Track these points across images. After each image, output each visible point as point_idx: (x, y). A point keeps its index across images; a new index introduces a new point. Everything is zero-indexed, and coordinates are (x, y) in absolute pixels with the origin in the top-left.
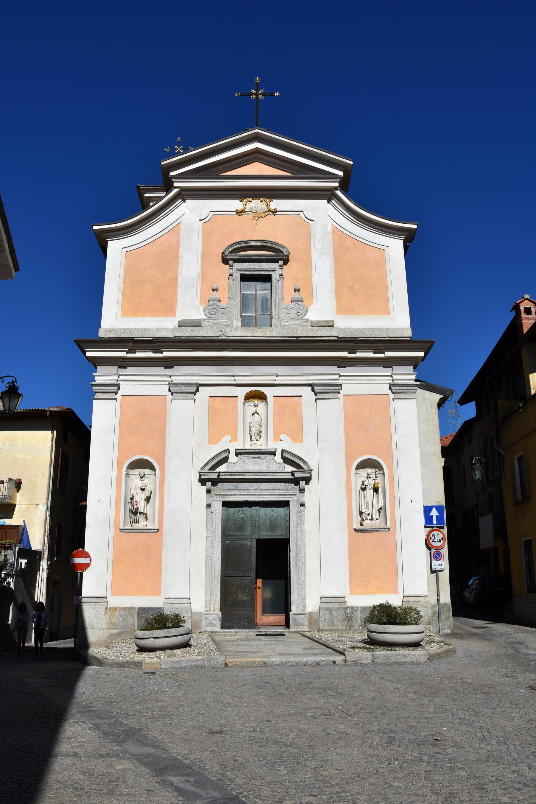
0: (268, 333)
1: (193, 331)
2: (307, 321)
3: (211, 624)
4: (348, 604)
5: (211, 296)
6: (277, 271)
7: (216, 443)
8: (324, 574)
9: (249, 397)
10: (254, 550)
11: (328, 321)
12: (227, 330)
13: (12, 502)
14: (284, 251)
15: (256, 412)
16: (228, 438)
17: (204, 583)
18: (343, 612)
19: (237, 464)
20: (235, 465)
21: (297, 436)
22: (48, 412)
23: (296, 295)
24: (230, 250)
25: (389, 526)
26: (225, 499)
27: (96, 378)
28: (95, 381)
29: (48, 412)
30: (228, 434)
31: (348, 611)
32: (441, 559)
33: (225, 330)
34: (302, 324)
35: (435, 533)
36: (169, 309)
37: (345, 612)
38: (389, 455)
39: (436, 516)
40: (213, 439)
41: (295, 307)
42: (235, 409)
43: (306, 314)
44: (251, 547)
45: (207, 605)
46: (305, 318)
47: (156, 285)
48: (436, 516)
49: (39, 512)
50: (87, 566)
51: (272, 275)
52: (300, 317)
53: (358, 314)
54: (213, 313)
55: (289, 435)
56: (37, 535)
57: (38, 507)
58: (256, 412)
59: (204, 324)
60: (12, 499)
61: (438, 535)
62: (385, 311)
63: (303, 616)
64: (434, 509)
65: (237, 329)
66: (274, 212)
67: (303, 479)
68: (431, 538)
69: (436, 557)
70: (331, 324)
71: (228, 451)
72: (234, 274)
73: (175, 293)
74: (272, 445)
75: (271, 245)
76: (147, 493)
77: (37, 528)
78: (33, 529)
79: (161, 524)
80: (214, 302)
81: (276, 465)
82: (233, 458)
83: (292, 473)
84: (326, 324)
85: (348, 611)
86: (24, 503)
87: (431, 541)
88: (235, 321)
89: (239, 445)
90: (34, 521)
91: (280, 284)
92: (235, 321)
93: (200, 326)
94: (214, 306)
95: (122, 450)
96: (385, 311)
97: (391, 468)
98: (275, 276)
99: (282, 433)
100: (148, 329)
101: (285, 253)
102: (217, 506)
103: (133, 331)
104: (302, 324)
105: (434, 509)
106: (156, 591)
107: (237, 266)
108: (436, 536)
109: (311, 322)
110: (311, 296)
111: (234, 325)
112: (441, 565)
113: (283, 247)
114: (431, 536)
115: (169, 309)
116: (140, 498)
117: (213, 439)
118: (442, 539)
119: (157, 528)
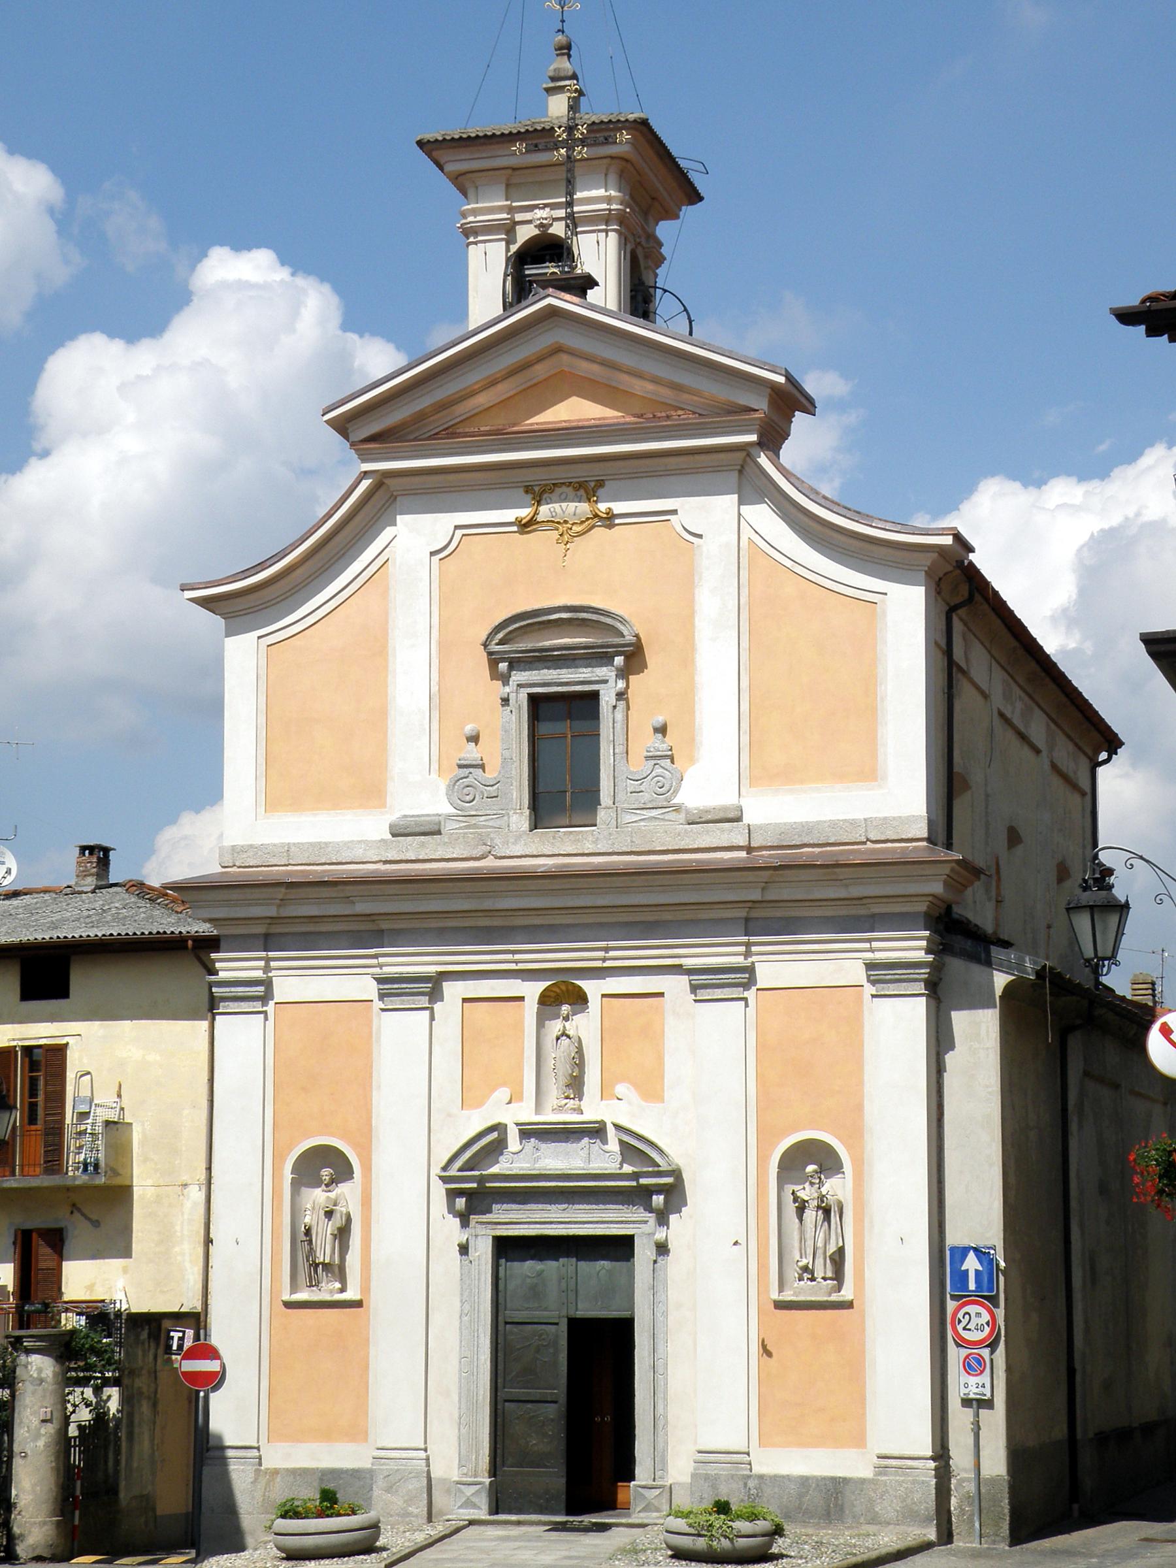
0: (588, 845)
1: (423, 845)
2: (678, 809)
3: (469, 1504)
4: (757, 1469)
5: (463, 755)
6: (612, 683)
7: (480, 1105)
8: (705, 1401)
9: (549, 1001)
10: (563, 1342)
11: (725, 809)
12: (498, 841)
13: (118, 1181)
14: (626, 633)
15: (564, 1034)
16: (503, 1094)
17: (456, 1416)
18: (741, 1484)
19: (521, 1155)
20: (519, 1159)
21: (651, 1088)
22: (190, 942)
23: (659, 744)
24: (500, 635)
25: (847, 1293)
26: (499, 1233)
27: (218, 965)
28: (216, 973)
29: (190, 942)
30: (504, 1084)
31: (751, 1484)
32: (982, 1372)
33: (492, 839)
34: (667, 817)
35: (972, 1309)
36: (371, 793)
37: (745, 1484)
38: (856, 1134)
39: (976, 1271)
40: (469, 1098)
41: (654, 774)
42: (519, 1026)
43: (676, 792)
44: (557, 1336)
45: (463, 1463)
46: (676, 801)
47: (327, 749)
48: (976, 1271)
49: (188, 1205)
50: (216, 1380)
51: (601, 692)
52: (664, 802)
53: (802, 782)
54: (468, 798)
55: (637, 1086)
56: (187, 1265)
57: (185, 1191)
58: (564, 1034)
59: (448, 827)
60: (115, 1173)
61: (978, 1315)
62: (868, 772)
63: (658, 1492)
64: (972, 1254)
65: (518, 838)
66: (609, 520)
67: (659, 1189)
68: (960, 1321)
69: (979, 1363)
70: (731, 815)
71: (499, 1128)
72: (512, 697)
73: (382, 746)
74: (592, 1110)
75: (594, 617)
76: (338, 1221)
77: (186, 1246)
78: (177, 1249)
79: (366, 1288)
80: (471, 770)
81: (604, 1159)
82: (514, 1142)
83: (635, 1176)
84: (721, 815)
85: (751, 1484)
86: (149, 1182)
87: (960, 1328)
88: (514, 818)
89: (525, 1112)
90: (178, 1228)
91: (619, 716)
92: (514, 818)
93: (439, 833)
94: (470, 780)
95: (282, 1126)
96: (868, 772)
97: (858, 1164)
98: (607, 698)
99: (622, 1081)
100: (326, 843)
101: (629, 638)
102: (483, 1250)
103: (293, 849)
104: (667, 817)
105: (972, 1254)
106: (357, 1432)
107: (518, 677)
108: (973, 1316)
109: (688, 812)
110: (691, 741)
111: (513, 827)
112: (983, 1386)
113: (623, 621)
114: (960, 1315)
115: (371, 793)
116: (324, 1233)
117: (469, 1098)
118: (988, 1323)
119: (357, 1297)
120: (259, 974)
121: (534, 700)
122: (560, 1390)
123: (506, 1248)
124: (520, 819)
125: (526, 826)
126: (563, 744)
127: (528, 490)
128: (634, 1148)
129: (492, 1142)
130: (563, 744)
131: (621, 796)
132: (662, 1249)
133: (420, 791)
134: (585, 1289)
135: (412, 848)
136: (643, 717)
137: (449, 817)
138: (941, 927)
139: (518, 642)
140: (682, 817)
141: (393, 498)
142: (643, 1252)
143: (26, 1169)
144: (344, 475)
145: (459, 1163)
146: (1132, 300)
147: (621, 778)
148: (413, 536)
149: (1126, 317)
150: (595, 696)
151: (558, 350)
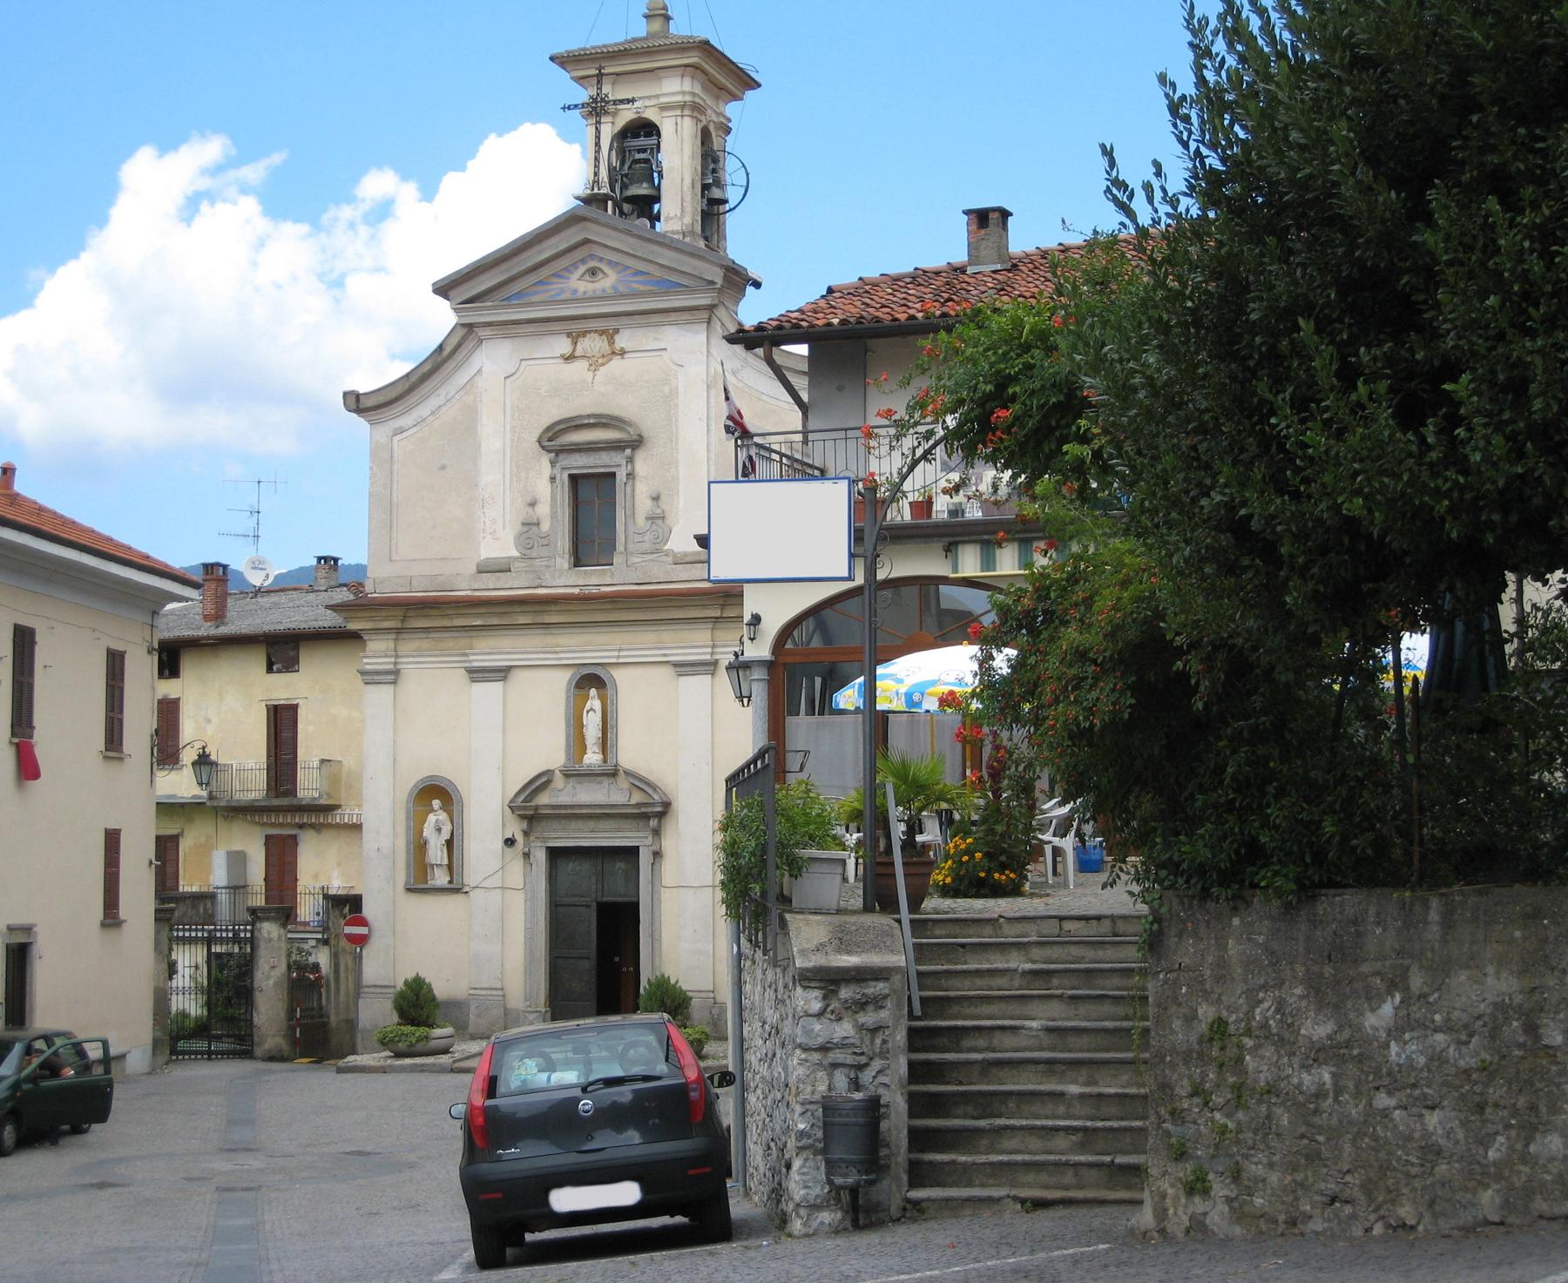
20: (563, 794)
59: (516, 566)
88: (559, 560)
92: (559, 560)
98: (621, 476)
102: (540, 856)
109: (675, 555)
120: (391, 667)
121: (574, 479)
122: (594, 955)
123: (555, 854)
124: (564, 562)
125: (566, 566)
126: (592, 505)
127: (569, 335)
128: (639, 782)
129: (541, 782)
130: (592, 505)
131: (630, 546)
132: (657, 854)
133: (500, 544)
134: (615, 892)
135: (490, 581)
136: (642, 490)
137: (516, 558)
138: (1146, 804)
139: (556, 439)
140: (670, 559)
141: (481, 341)
142: (645, 858)
143: (861, 1217)
144: (442, 318)
145: (522, 798)
146: (560, 49)
147: (630, 532)
148: (492, 363)
149: (552, 59)
150: (613, 475)
151: (586, 241)
